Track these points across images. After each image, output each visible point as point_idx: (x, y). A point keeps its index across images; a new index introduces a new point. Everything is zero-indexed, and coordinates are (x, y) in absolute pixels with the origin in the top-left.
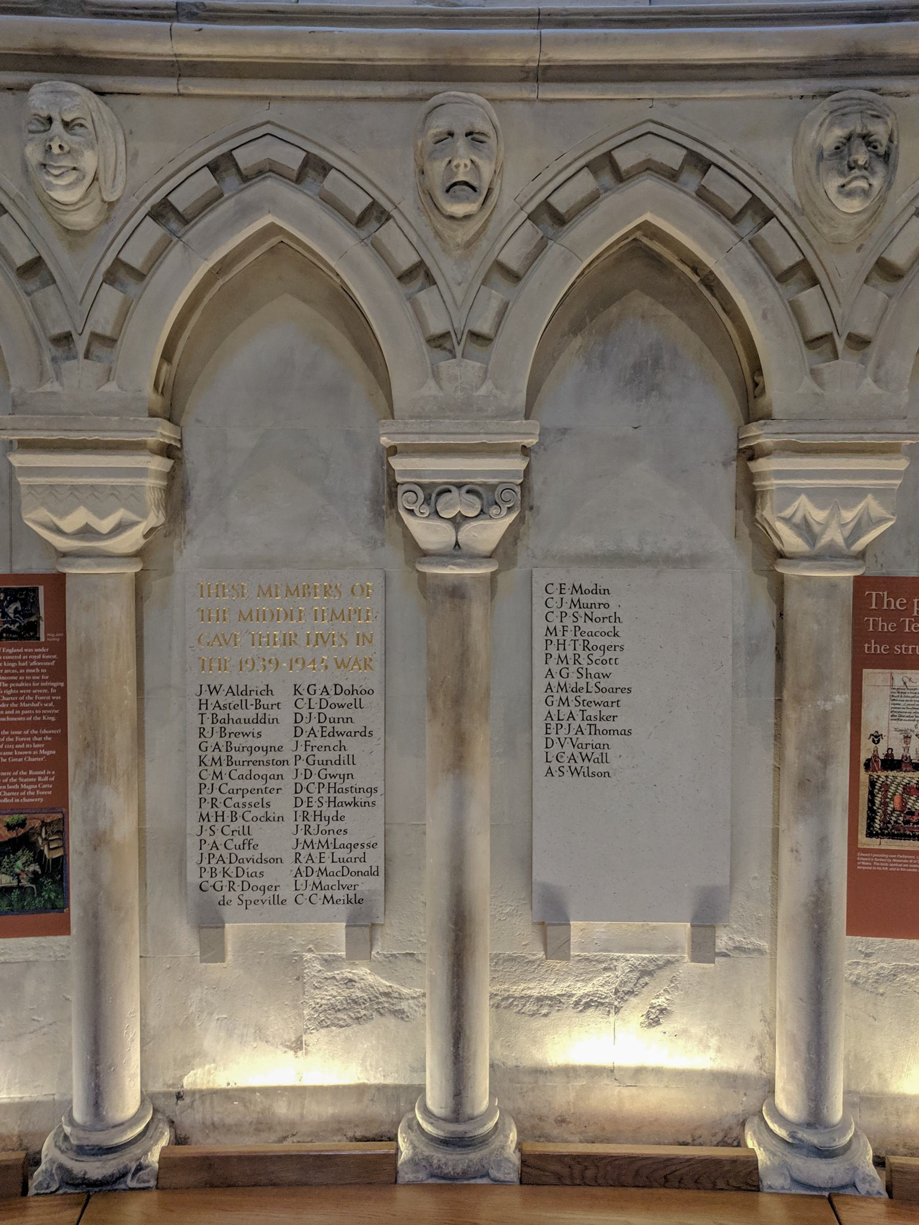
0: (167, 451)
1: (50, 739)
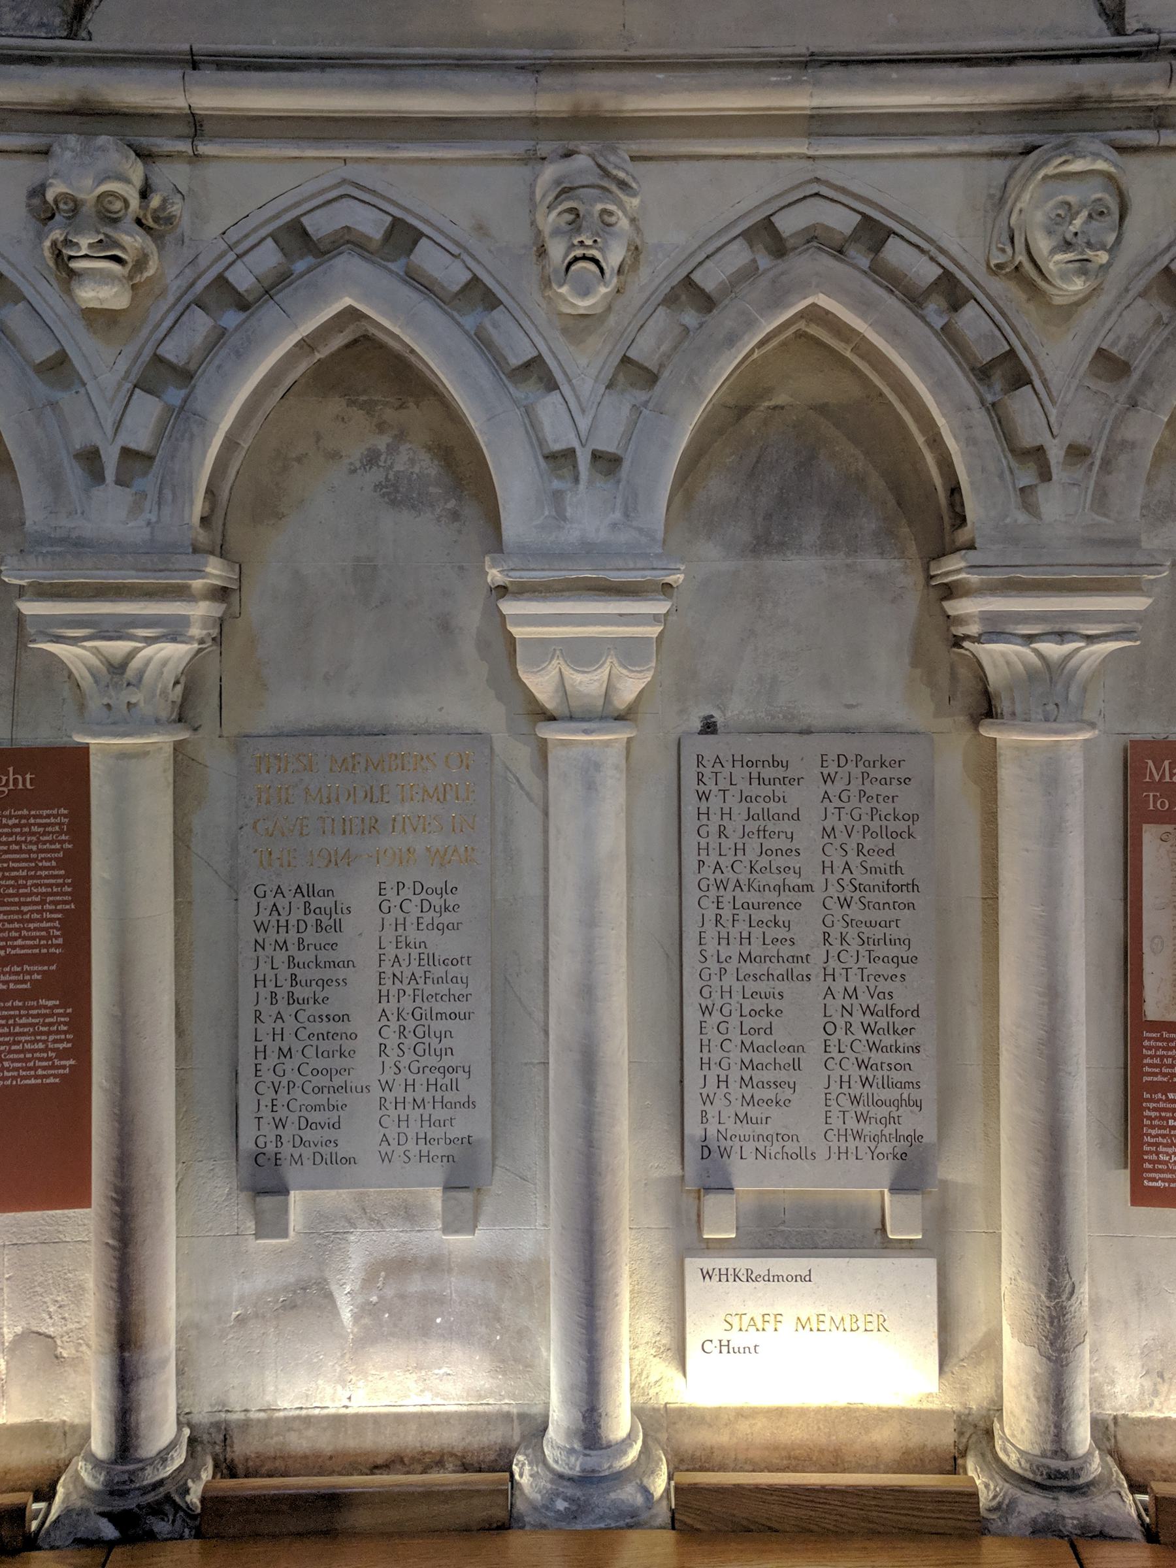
0: (221, 594)
1: (39, 977)
